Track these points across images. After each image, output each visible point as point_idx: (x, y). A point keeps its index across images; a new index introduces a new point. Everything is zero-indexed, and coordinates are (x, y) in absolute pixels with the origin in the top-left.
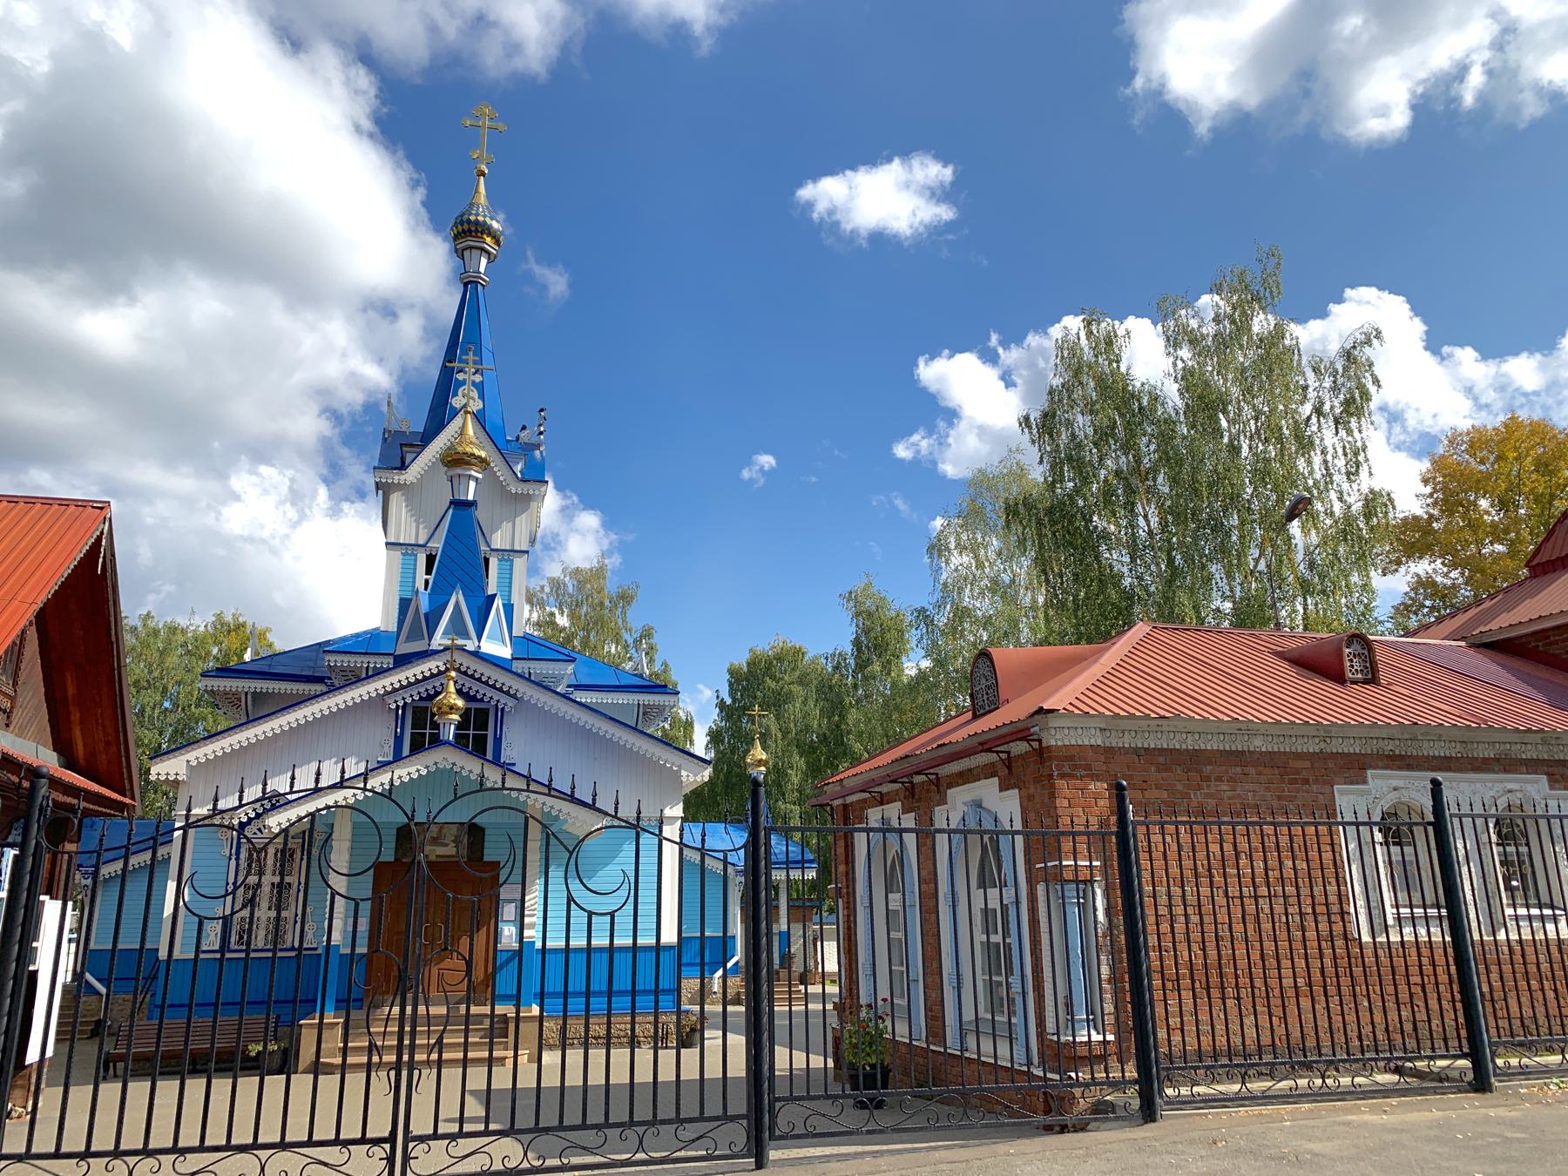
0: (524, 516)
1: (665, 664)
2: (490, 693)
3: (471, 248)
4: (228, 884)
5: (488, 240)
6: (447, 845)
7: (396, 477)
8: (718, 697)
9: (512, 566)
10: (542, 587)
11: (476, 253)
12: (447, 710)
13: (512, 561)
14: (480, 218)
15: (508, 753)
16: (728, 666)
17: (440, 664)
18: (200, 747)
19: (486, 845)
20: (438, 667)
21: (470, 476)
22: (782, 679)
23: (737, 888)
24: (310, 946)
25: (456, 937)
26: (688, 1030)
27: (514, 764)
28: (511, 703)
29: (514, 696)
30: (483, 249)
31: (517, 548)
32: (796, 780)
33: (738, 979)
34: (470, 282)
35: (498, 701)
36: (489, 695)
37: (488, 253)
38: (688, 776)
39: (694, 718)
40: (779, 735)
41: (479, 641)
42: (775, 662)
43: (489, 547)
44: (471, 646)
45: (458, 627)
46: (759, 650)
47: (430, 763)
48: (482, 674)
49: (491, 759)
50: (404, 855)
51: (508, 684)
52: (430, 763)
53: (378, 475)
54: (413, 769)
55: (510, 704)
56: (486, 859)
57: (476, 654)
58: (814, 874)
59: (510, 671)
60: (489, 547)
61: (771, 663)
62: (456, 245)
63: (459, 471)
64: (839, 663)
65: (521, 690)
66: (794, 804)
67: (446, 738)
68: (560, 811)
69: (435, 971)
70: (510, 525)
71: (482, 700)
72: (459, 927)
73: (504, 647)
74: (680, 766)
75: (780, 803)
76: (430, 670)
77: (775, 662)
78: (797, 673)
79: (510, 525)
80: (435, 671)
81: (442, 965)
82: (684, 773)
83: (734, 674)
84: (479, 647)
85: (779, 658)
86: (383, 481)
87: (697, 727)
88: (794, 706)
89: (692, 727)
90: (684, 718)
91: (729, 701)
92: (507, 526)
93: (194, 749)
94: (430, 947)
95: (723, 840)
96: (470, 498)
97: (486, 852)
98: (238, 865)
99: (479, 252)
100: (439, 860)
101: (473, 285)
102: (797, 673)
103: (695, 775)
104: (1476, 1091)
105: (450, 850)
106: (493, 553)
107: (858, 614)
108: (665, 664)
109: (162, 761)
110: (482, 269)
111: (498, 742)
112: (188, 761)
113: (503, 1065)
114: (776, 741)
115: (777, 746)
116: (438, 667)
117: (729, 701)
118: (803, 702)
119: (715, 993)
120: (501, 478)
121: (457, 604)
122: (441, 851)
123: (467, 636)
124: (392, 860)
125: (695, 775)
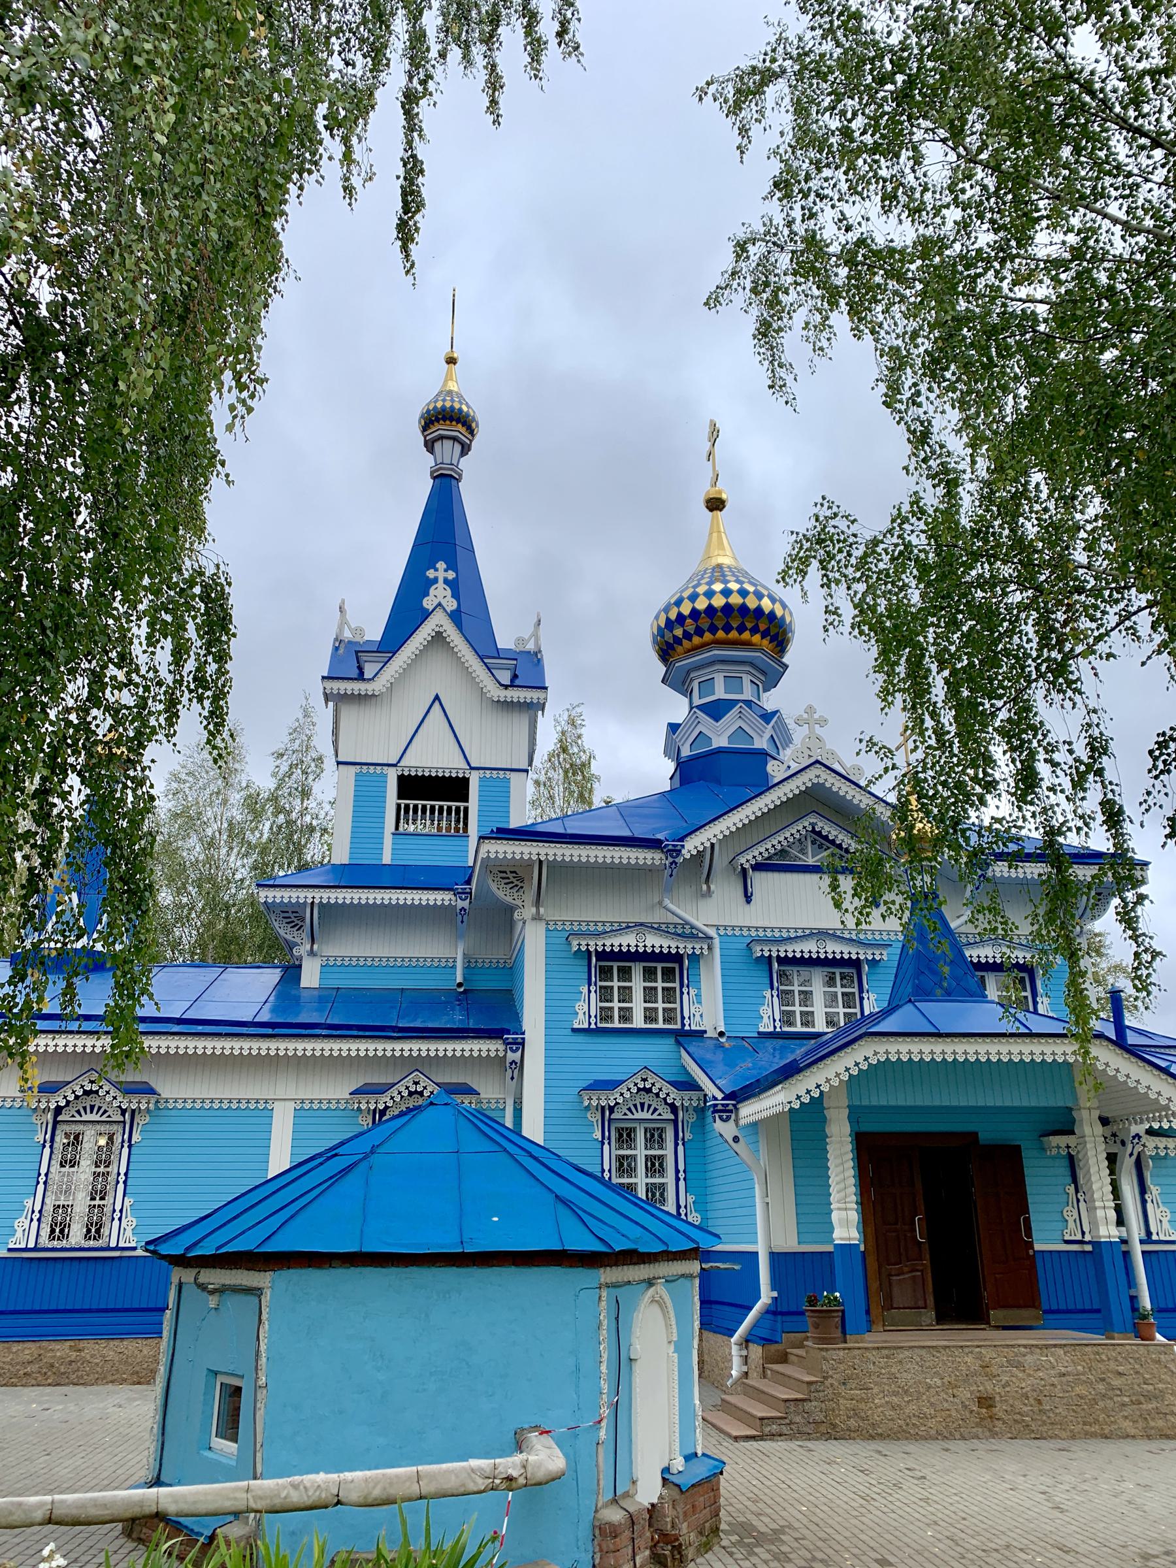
4: (39, 1175)
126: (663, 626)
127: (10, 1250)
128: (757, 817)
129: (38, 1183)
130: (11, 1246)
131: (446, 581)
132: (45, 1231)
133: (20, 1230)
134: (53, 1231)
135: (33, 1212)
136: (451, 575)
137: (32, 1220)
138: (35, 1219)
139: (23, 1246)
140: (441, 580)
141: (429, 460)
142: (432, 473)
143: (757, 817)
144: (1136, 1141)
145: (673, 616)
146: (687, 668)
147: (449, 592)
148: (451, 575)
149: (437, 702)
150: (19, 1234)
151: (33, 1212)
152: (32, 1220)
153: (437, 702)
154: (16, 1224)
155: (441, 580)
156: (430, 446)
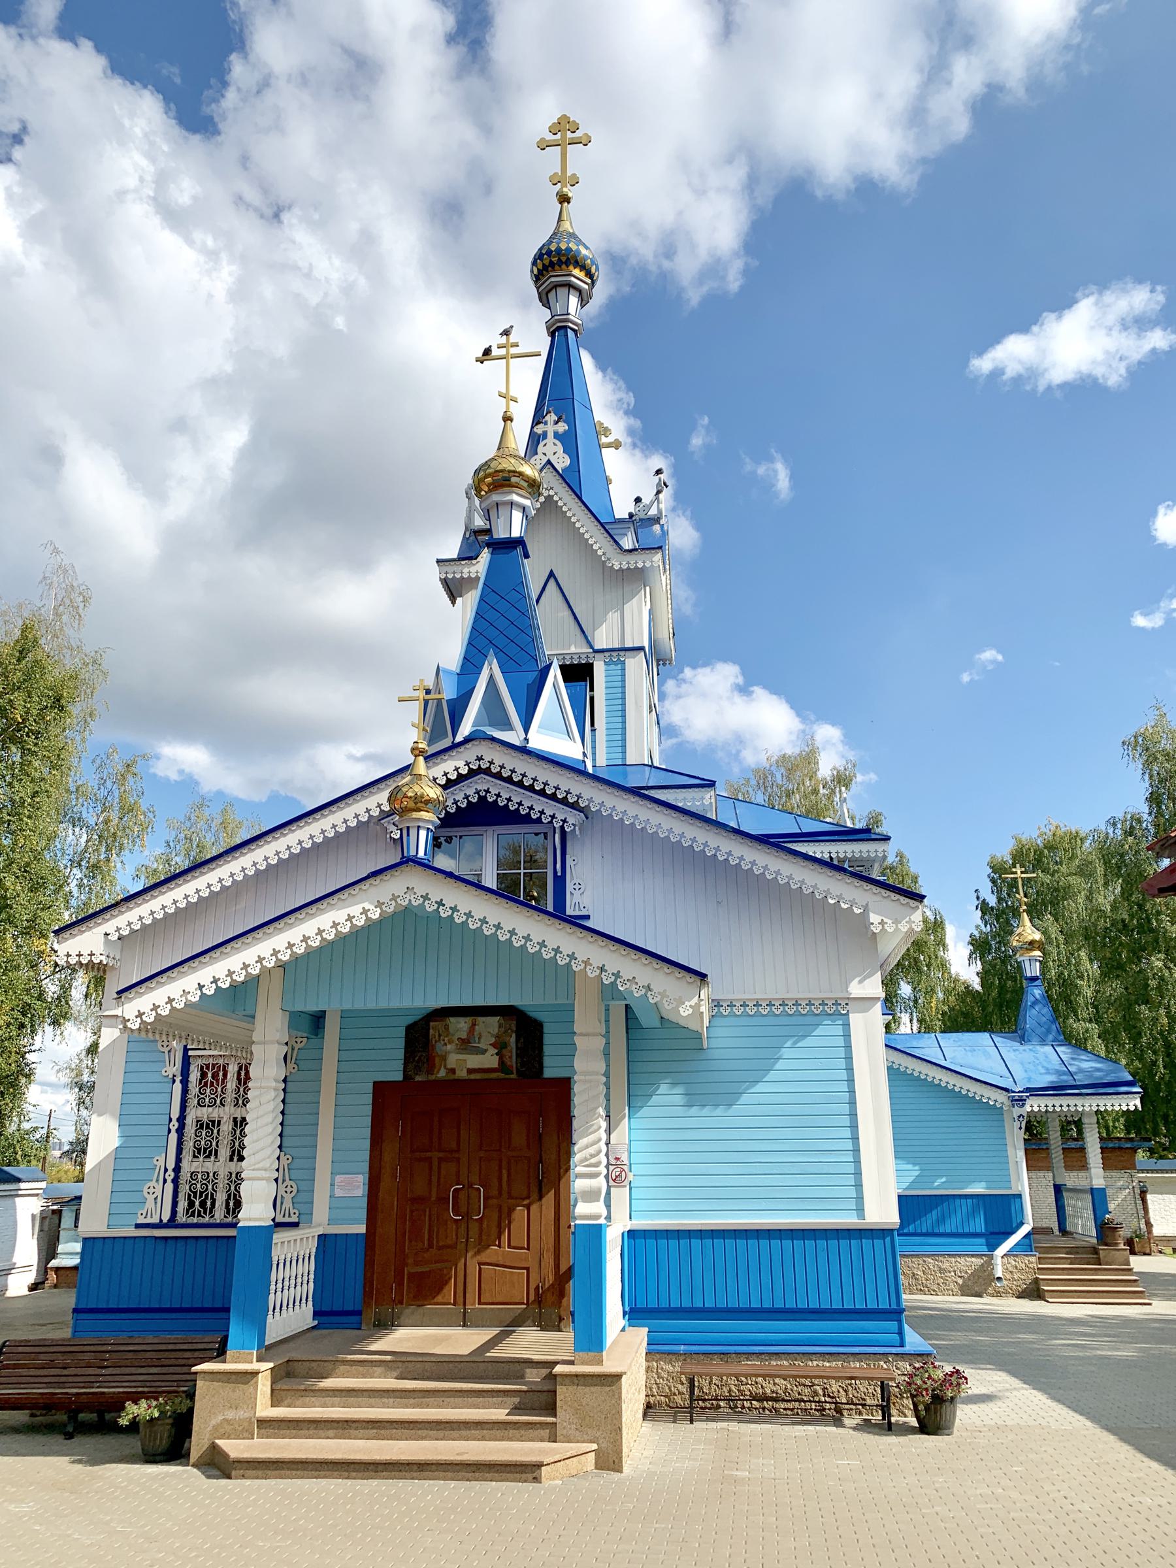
0: (635, 600)
1: (900, 855)
2: (550, 808)
3: (556, 286)
4: (170, 1120)
5: (576, 272)
6: (484, 1052)
7: (466, 570)
8: (978, 898)
9: (624, 669)
10: (748, 780)
11: (562, 292)
12: (412, 805)
13: (623, 663)
14: (563, 246)
15: (577, 897)
16: (988, 859)
17: (461, 764)
18: (122, 913)
19: (547, 1050)
20: (457, 769)
21: (512, 504)
22: (1057, 871)
23: (1017, 1124)
24: (287, 1220)
25: (505, 1210)
26: (928, 1399)
27: (587, 917)
28: (573, 818)
29: (574, 806)
30: (570, 286)
31: (628, 644)
32: (1089, 993)
33: (1033, 1259)
34: (559, 328)
35: (564, 821)
36: (549, 812)
37: (579, 291)
38: (882, 923)
39: (944, 918)
40: (1061, 939)
41: (526, 731)
42: (1046, 852)
43: (592, 647)
44: (514, 737)
45: (494, 711)
46: (1024, 838)
47: (385, 898)
48: (524, 775)
49: (552, 910)
50: (418, 1070)
51: (564, 788)
52: (385, 898)
53: (446, 569)
54: (355, 910)
55: (571, 820)
56: (548, 1073)
57: (524, 750)
58: (1138, 1102)
59: (583, 773)
60: (592, 647)
61: (1042, 853)
62: (538, 288)
63: (496, 497)
64: (1132, 827)
65: (586, 796)
66: (1090, 1021)
67: (413, 853)
68: (617, 975)
69: (473, 1269)
70: (617, 615)
71: (539, 821)
72: (509, 1193)
73: (571, 743)
74: (866, 909)
75: (1071, 1021)
76: (446, 774)
77: (1046, 852)
78: (1077, 862)
79: (617, 615)
80: (453, 776)
81: (483, 1257)
82: (874, 918)
83: (998, 870)
84: (526, 740)
85: (1051, 847)
86: (450, 576)
87: (950, 932)
88: (1075, 902)
89: (943, 929)
90: (932, 918)
91: (992, 901)
92: (613, 617)
93: (114, 917)
94: (463, 1226)
95: (987, 1055)
96: (516, 533)
97: (547, 1061)
98: (185, 1091)
99: (565, 290)
100: (473, 1077)
101: (562, 332)
102: (1077, 862)
103: (896, 922)
104: (888, 1068)
105: (490, 1060)
106: (597, 655)
107: (1148, 764)
108: (900, 855)
109: (73, 936)
110: (572, 310)
111: (560, 881)
112: (107, 934)
113: (537, 1480)
114: (1058, 946)
115: (1058, 954)
116: (457, 769)
117: (992, 901)
118: (1087, 898)
119: (999, 1279)
120: (600, 553)
121: (491, 680)
122: (474, 1061)
123: (507, 725)
124: (399, 1077)
125: (896, 922)
126: (541, 268)
127: (138, 1226)
128: (939, 1085)
129: (169, 1131)
130: (141, 1220)
131: (557, 435)
132: (182, 1205)
133: (151, 1198)
134: (191, 1204)
135: (166, 1170)
136: (562, 427)
137: (165, 1181)
138: (169, 1179)
139: (156, 1220)
140: (551, 435)
141: (546, 314)
142: (548, 329)
143: (939, 1085)
144: (1021, 1119)
145: (536, 271)
146: (555, 283)
147: (560, 448)
148: (562, 427)
149: (552, 581)
150: (150, 1203)
151: (166, 1170)
152: (165, 1181)
153: (552, 581)
154: (145, 1190)
155: (551, 435)
156: (545, 300)
